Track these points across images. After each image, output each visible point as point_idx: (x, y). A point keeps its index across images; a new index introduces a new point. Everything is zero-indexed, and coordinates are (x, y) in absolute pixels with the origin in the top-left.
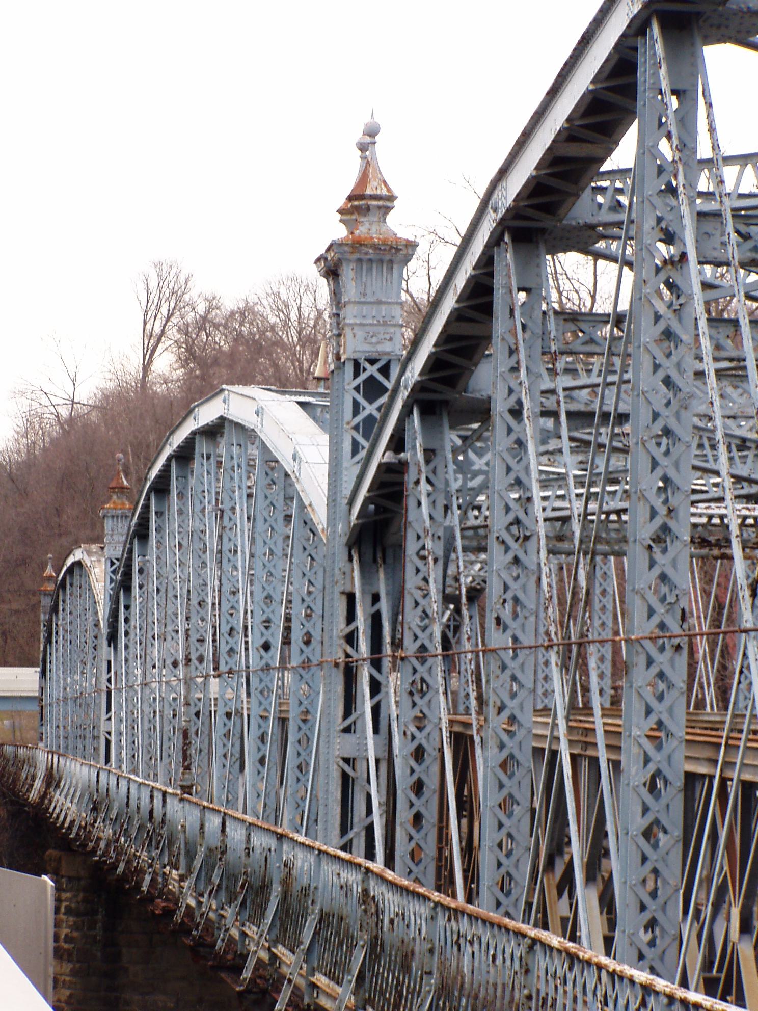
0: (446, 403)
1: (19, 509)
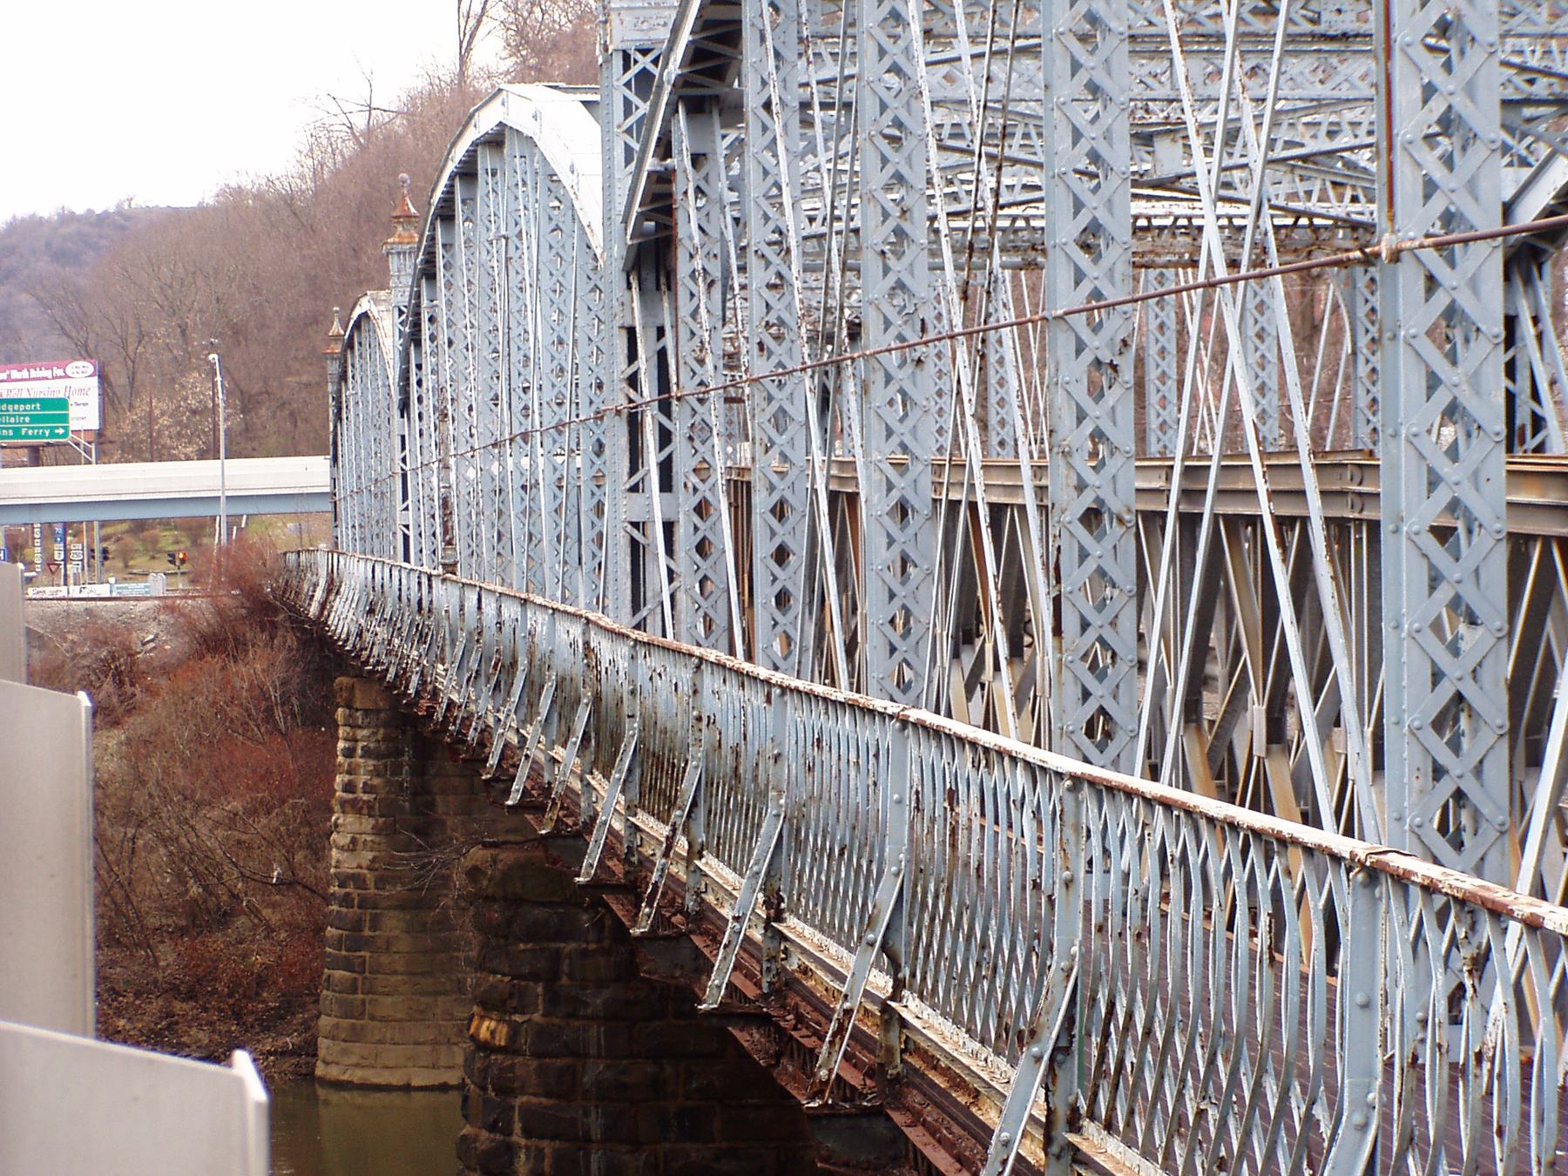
0: (716, 98)
1: (306, 252)
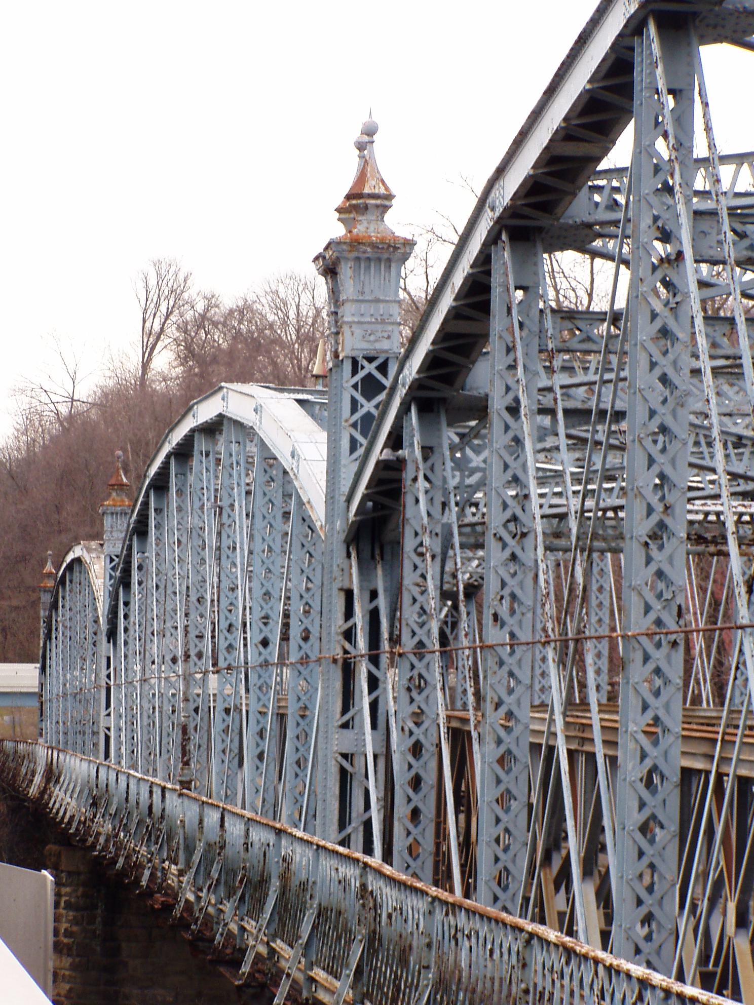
0: (444, 400)
1: (19, 506)
